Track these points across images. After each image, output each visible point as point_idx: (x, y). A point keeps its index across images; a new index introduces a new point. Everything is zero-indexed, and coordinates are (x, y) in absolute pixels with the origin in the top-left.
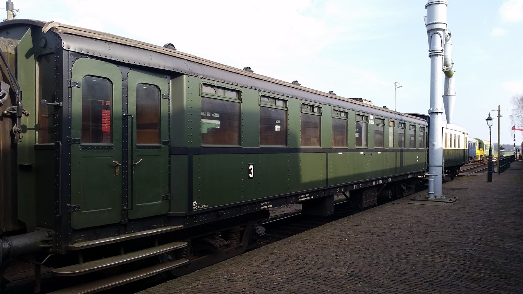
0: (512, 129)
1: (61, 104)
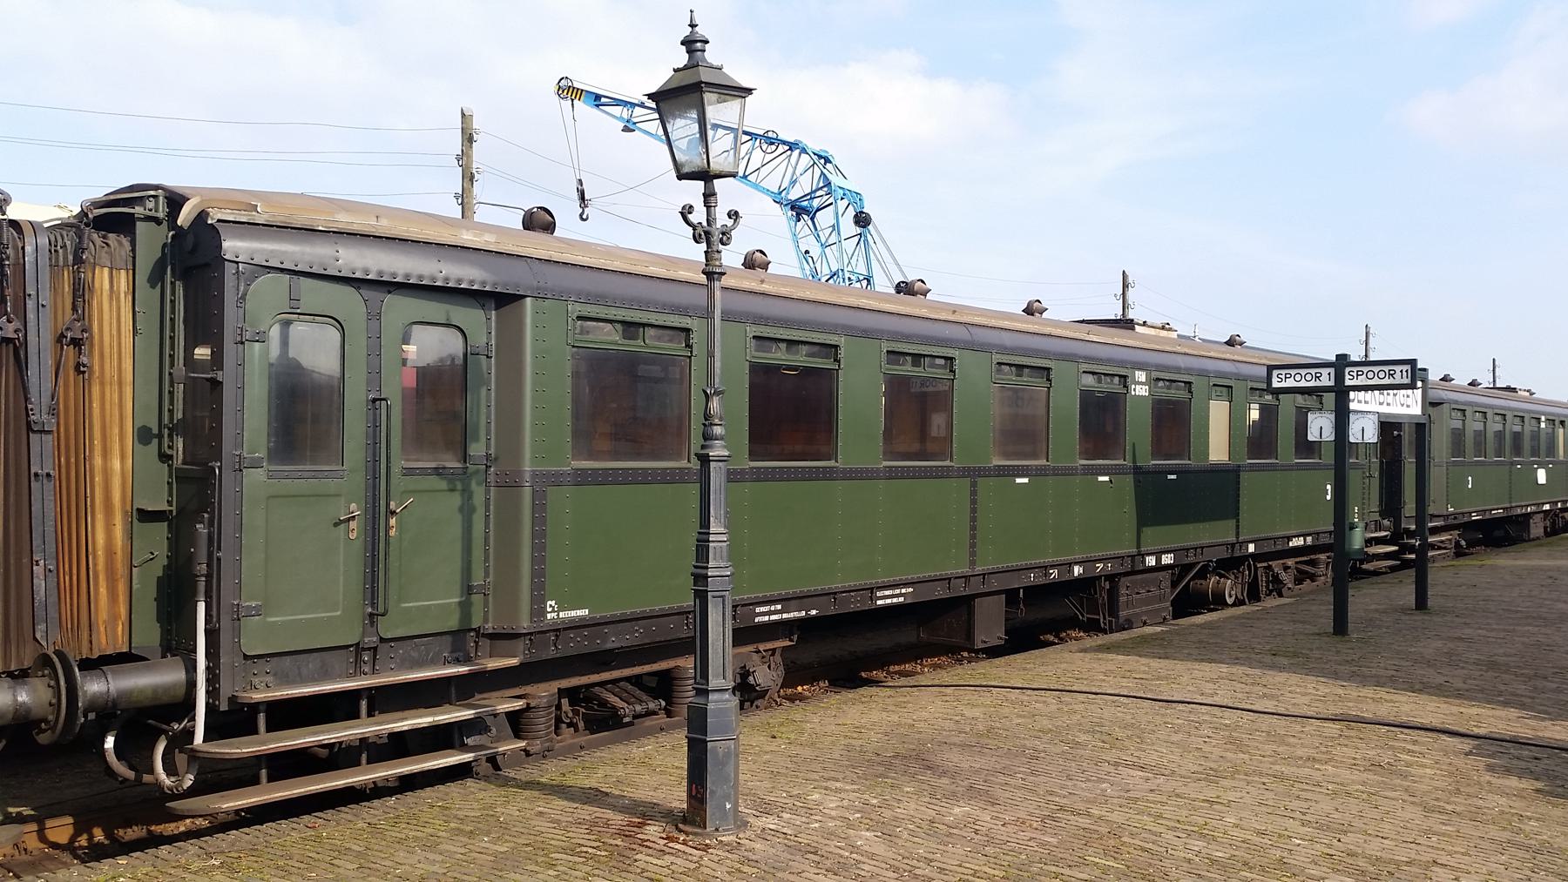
0: (736, 213)
1: (220, 376)
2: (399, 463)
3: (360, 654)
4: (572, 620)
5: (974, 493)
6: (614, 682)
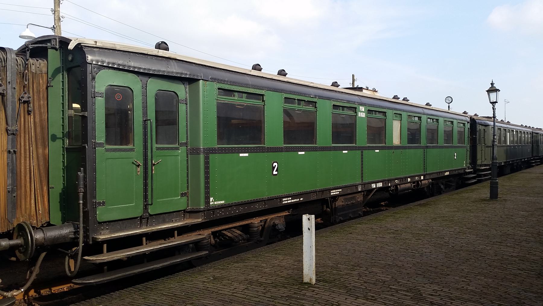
1: (86, 114)
2: (155, 146)
3: (142, 220)
4: (219, 205)
5: (362, 155)
6: (230, 228)
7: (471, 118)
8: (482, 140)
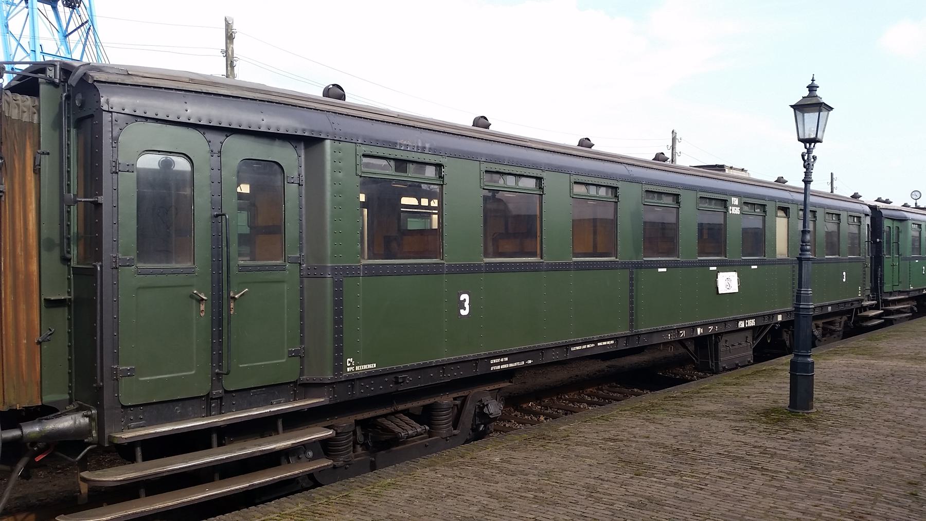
1: (100, 199)
3: (209, 403)
5: (631, 279)
7: (870, 207)
8: (893, 246)
